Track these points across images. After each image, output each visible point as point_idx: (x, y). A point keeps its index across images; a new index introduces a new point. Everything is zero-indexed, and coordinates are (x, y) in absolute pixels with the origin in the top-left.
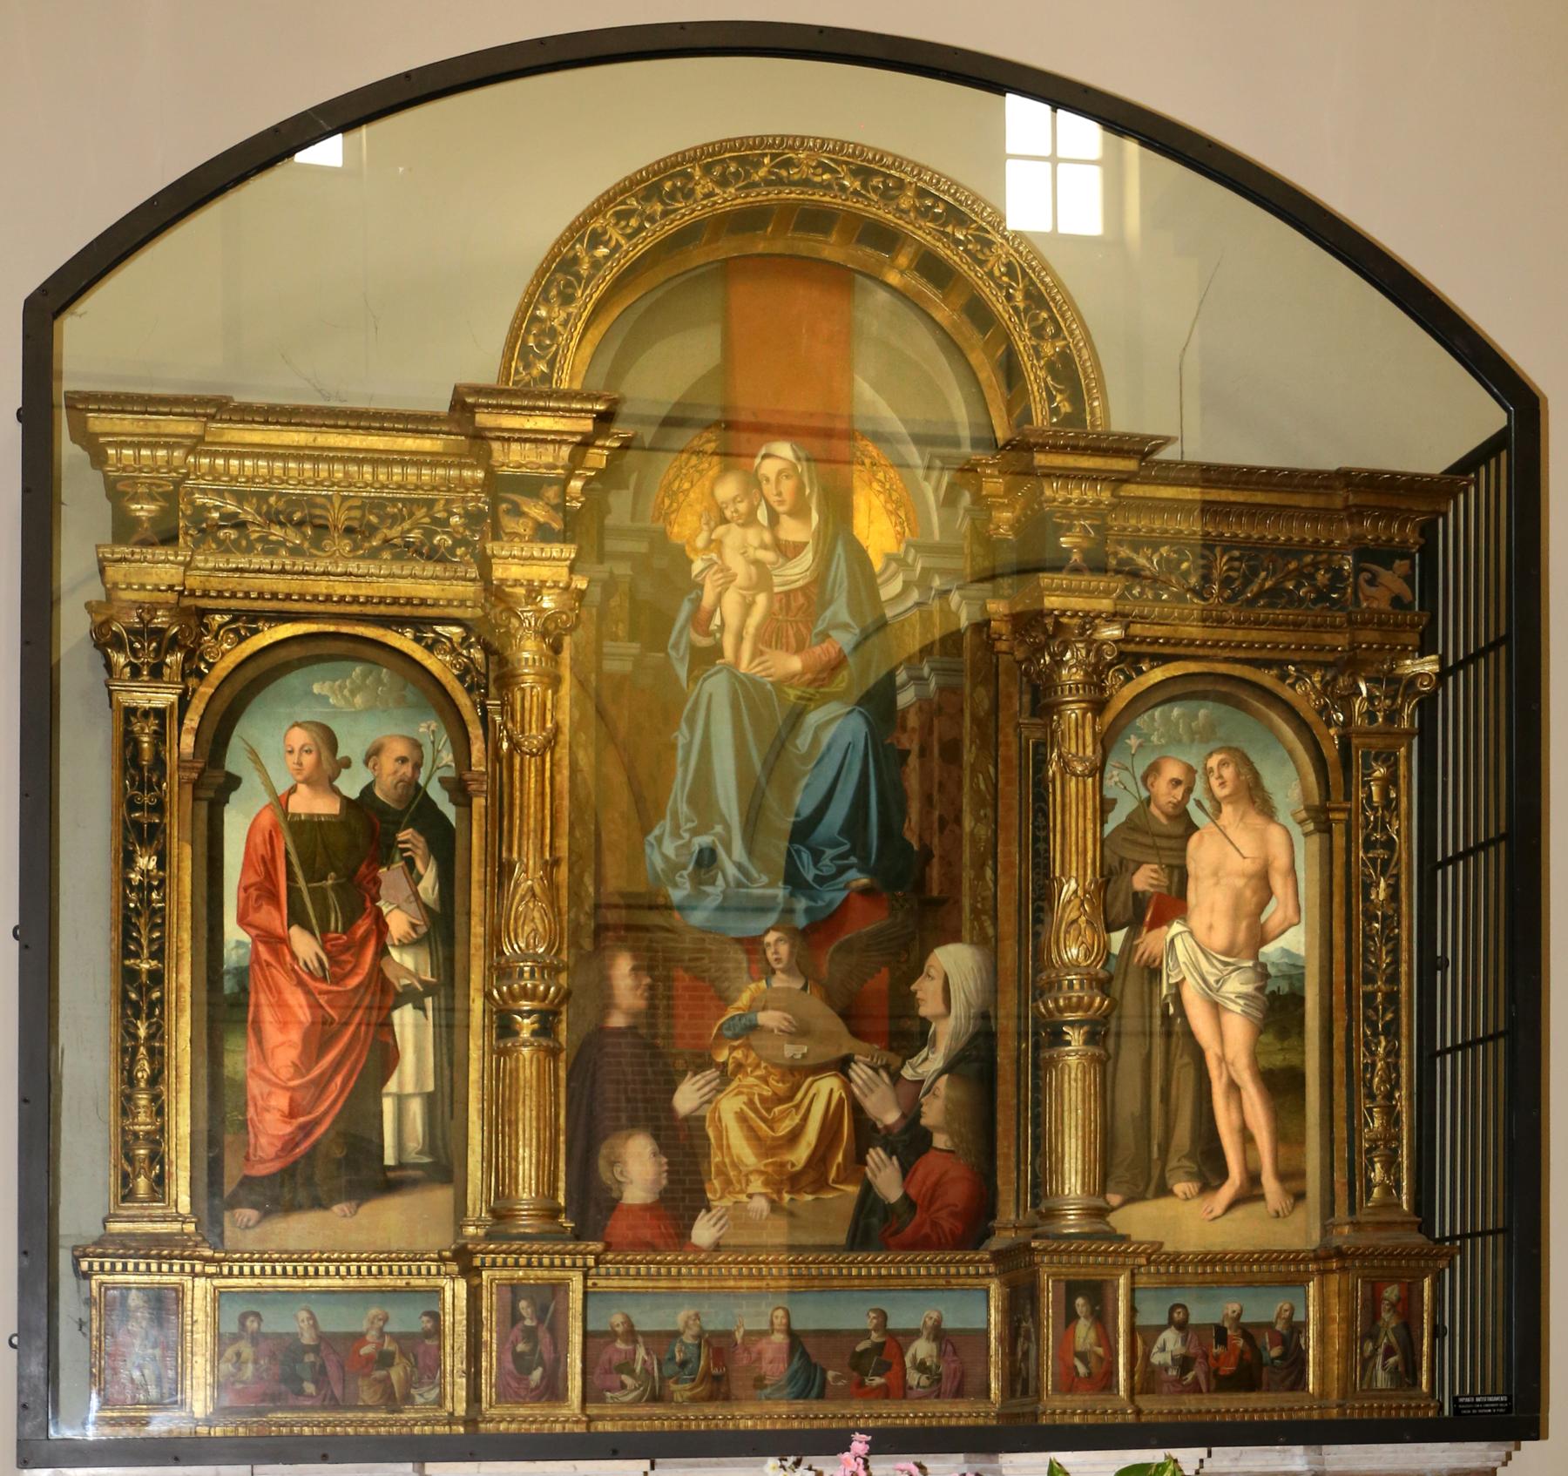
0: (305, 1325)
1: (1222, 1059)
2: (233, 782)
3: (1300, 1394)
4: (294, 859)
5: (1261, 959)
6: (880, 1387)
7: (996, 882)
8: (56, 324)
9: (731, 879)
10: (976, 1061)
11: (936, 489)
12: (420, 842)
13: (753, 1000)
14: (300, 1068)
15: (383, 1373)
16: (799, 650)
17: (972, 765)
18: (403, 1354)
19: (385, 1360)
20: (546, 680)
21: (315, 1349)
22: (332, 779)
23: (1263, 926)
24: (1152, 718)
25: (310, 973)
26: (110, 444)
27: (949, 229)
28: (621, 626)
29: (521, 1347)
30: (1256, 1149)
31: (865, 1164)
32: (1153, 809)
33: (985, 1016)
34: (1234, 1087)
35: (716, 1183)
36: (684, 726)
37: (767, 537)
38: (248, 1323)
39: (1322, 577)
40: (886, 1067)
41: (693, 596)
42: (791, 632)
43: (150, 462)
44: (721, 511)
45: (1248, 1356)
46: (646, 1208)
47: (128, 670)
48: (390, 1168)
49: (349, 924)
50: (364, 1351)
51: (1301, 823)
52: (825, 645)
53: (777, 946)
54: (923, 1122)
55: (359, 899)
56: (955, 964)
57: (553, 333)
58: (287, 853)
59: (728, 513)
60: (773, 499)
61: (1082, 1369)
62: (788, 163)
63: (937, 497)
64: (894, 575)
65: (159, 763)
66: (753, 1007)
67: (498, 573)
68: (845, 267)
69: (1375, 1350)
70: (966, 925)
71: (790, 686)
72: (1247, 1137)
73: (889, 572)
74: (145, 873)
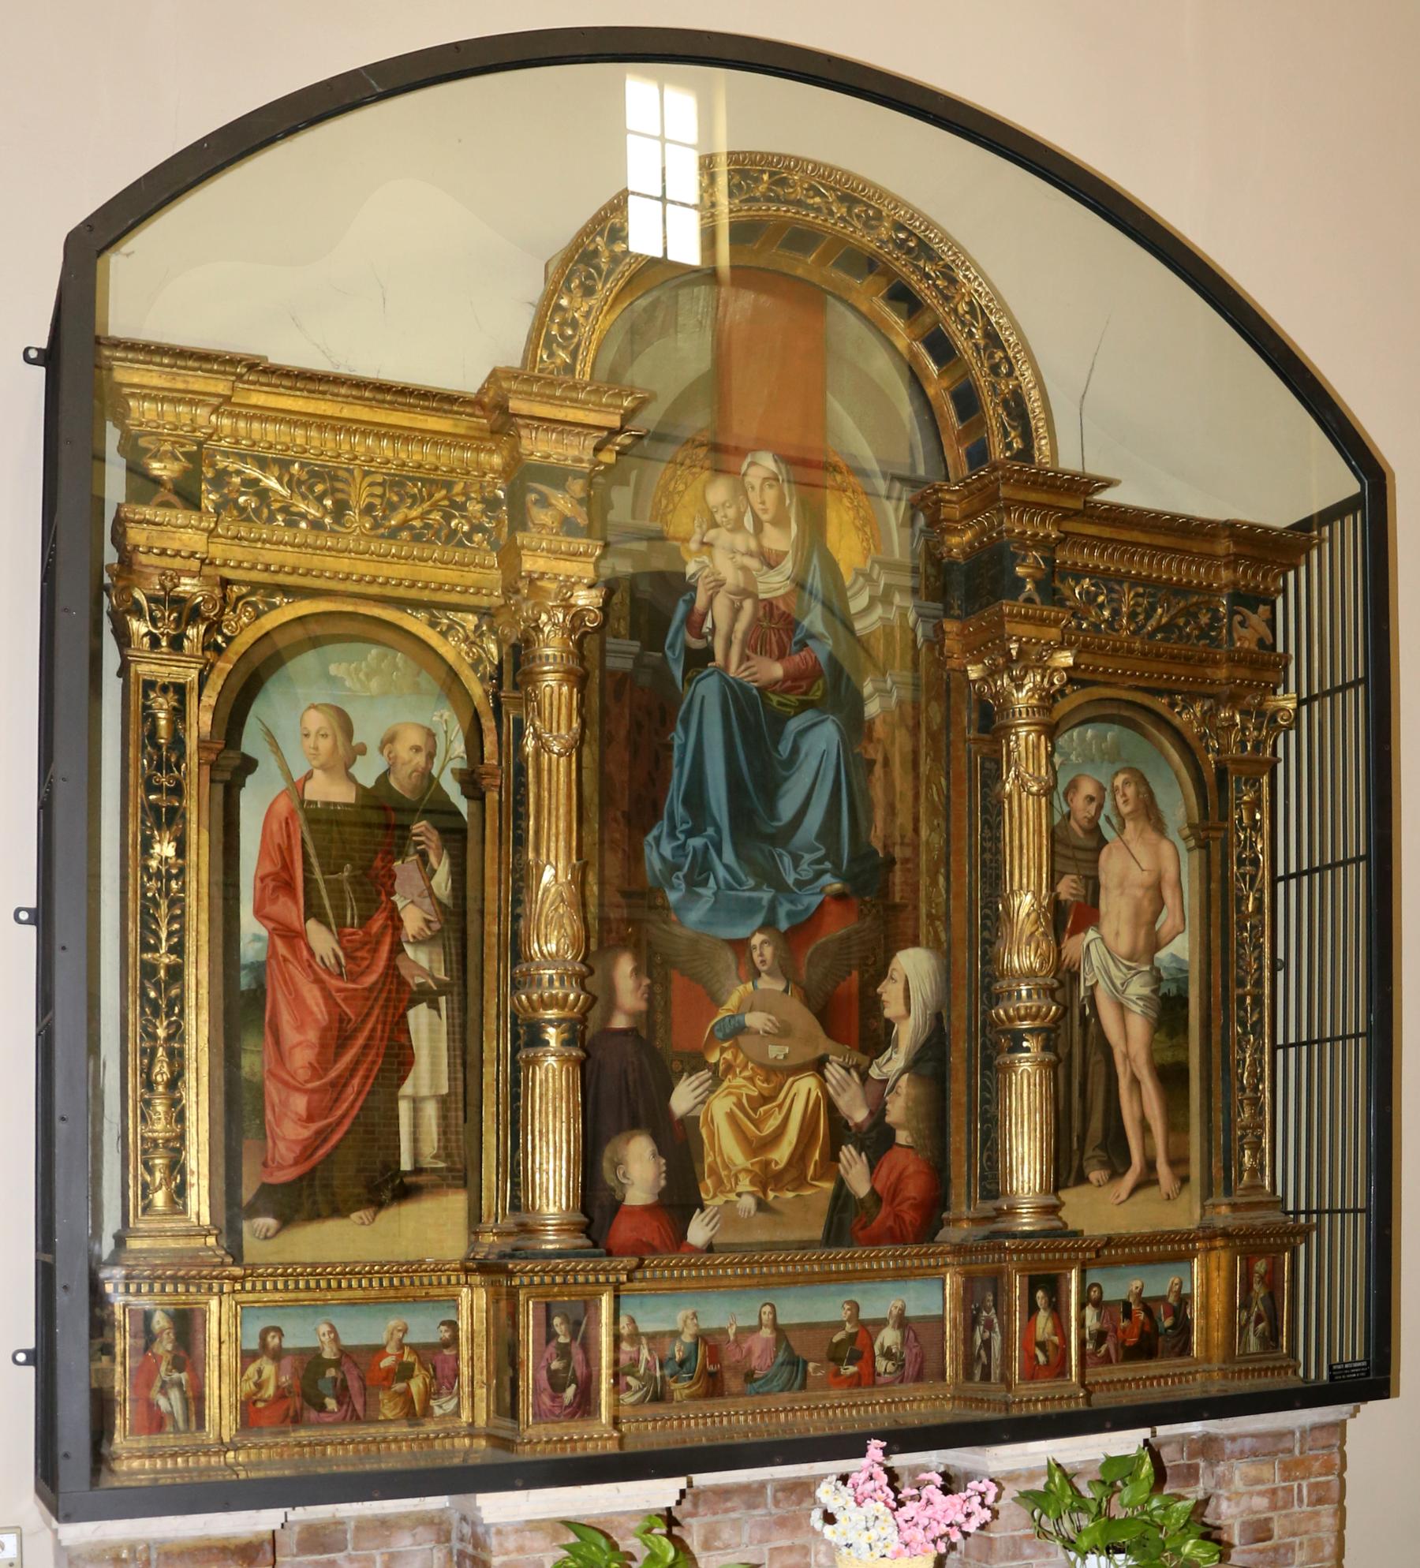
0: (326, 1339)
1: (1126, 1056)
2: (249, 765)
3: (1186, 1360)
4: (311, 851)
5: (1156, 964)
6: (852, 1375)
7: (948, 891)
8: (100, 262)
9: (722, 883)
10: (931, 1059)
11: (897, 510)
12: (434, 836)
13: (741, 1001)
14: (319, 1068)
15: (404, 1385)
16: (781, 657)
17: (928, 777)
18: (423, 1365)
19: (404, 1372)
20: (572, 678)
21: (337, 1364)
22: (347, 767)
23: (1157, 934)
24: (1071, 739)
25: (327, 970)
26: (133, 395)
27: (921, 264)
28: (622, 623)
29: (556, 1365)
30: (1152, 1138)
31: (838, 1160)
32: (1073, 823)
33: (938, 1017)
34: (1135, 1082)
35: (709, 1182)
36: (679, 727)
37: (753, 545)
38: (269, 1339)
39: (1204, 619)
40: (857, 1067)
41: (687, 597)
42: (774, 639)
43: (172, 419)
44: (712, 514)
45: (1147, 1328)
46: (646, 1209)
47: (146, 640)
48: (406, 1173)
49: (365, 919)
50: (386, 1363)
51: (1185, 839)
52: (803, 654)
53: (762, 948)
54: (888, 1119)
55: (375, 890)
56: (914, 966)
57: (574, 325)
58: (303, 841)
59: (718, 517)
60: (758, 507)
61: (1041, 1358)
62: (783, 182)
63: (897, 519)
64: (861, 589)
65: (178, 742)
66: (741, 1011)
67: (529, 564)
68: (818, 287)
69: (1249, 1318)
70: (923, 931)
71: (774, 692)
72: (1145, 1128)
73: (857, 587)
74: (164, 861)
